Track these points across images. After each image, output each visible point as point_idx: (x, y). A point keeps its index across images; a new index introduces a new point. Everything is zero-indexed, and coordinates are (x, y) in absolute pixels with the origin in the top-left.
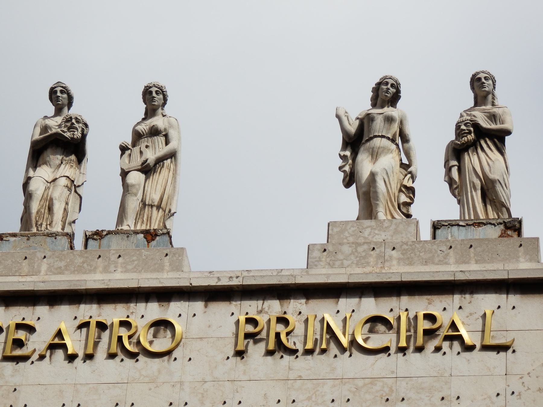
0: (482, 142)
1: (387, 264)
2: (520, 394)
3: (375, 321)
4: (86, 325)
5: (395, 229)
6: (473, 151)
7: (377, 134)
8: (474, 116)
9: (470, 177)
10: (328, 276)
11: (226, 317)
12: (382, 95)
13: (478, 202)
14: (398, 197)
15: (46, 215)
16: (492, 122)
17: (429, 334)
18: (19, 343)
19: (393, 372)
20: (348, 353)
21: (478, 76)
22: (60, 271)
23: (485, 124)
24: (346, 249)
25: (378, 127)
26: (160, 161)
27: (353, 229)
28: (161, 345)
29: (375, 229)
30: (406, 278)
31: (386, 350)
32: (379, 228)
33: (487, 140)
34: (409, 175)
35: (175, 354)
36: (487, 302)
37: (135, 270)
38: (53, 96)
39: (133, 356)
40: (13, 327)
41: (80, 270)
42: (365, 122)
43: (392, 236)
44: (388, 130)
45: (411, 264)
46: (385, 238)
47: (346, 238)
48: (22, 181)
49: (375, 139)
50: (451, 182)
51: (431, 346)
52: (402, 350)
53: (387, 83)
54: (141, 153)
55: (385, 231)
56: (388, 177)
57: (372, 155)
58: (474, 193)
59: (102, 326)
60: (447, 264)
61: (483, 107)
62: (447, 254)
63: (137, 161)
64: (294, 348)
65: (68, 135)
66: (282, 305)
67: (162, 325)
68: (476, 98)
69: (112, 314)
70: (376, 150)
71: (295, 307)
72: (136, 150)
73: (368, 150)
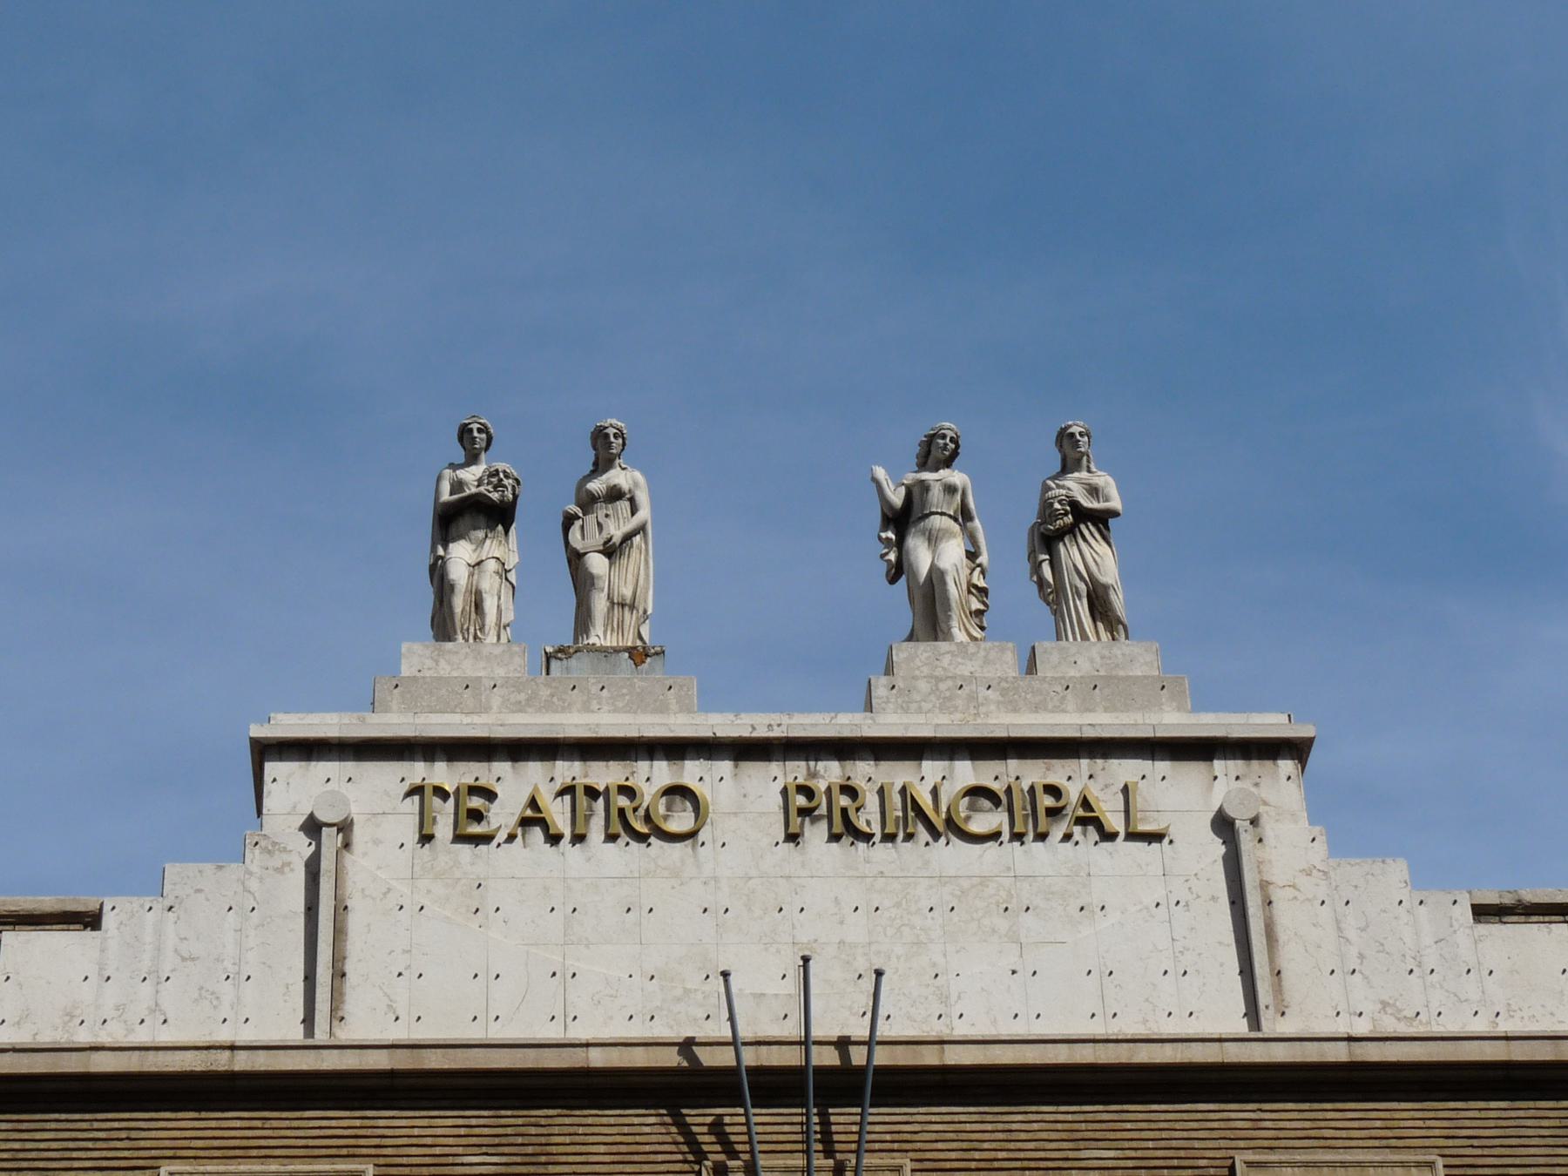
0: (1082, 527)
1: (982, 709)
2: (1187, 905)
3: (976, 792)
9: (1069, 578)
10: (907, 726)
11: (766, 783)
14: (968, 602)
15: (473, 615)
17: (1053, 813)
18: (476, 816)
19: (1009, 869)
20: (943, 840)
22: (520, 708)
23: (1087, 503)
24: (923, 686)
26: (628, 537)
28: (681, 821)
30: (1015, 734)
31: (995, 836)
35: (702, 836)
36: (1126, 769)
37: (627, 709)
38: (466, 436)
39: (641, 838)
40: (464, 791)
41: (548, 707)
44: (949, 504)
45: (1015, 710)
48: (427, 560)
50: (1041, 583)
51: (1058, 832)
52: (1018, 837)
53: (944, 436)
54: (600, 525)
57: (929, 540)
59: (592, 793)
60: (1064, 711)
61: (1076, 475)
62: (1064, 698)
63: (597, 540)
64: (867, 830)
65: (495, 496)
66: (843, 767)
67: (678, 792)
68: (1064, 460)
69: (605, 774)
71: (863, 771)
72: (590, 520)
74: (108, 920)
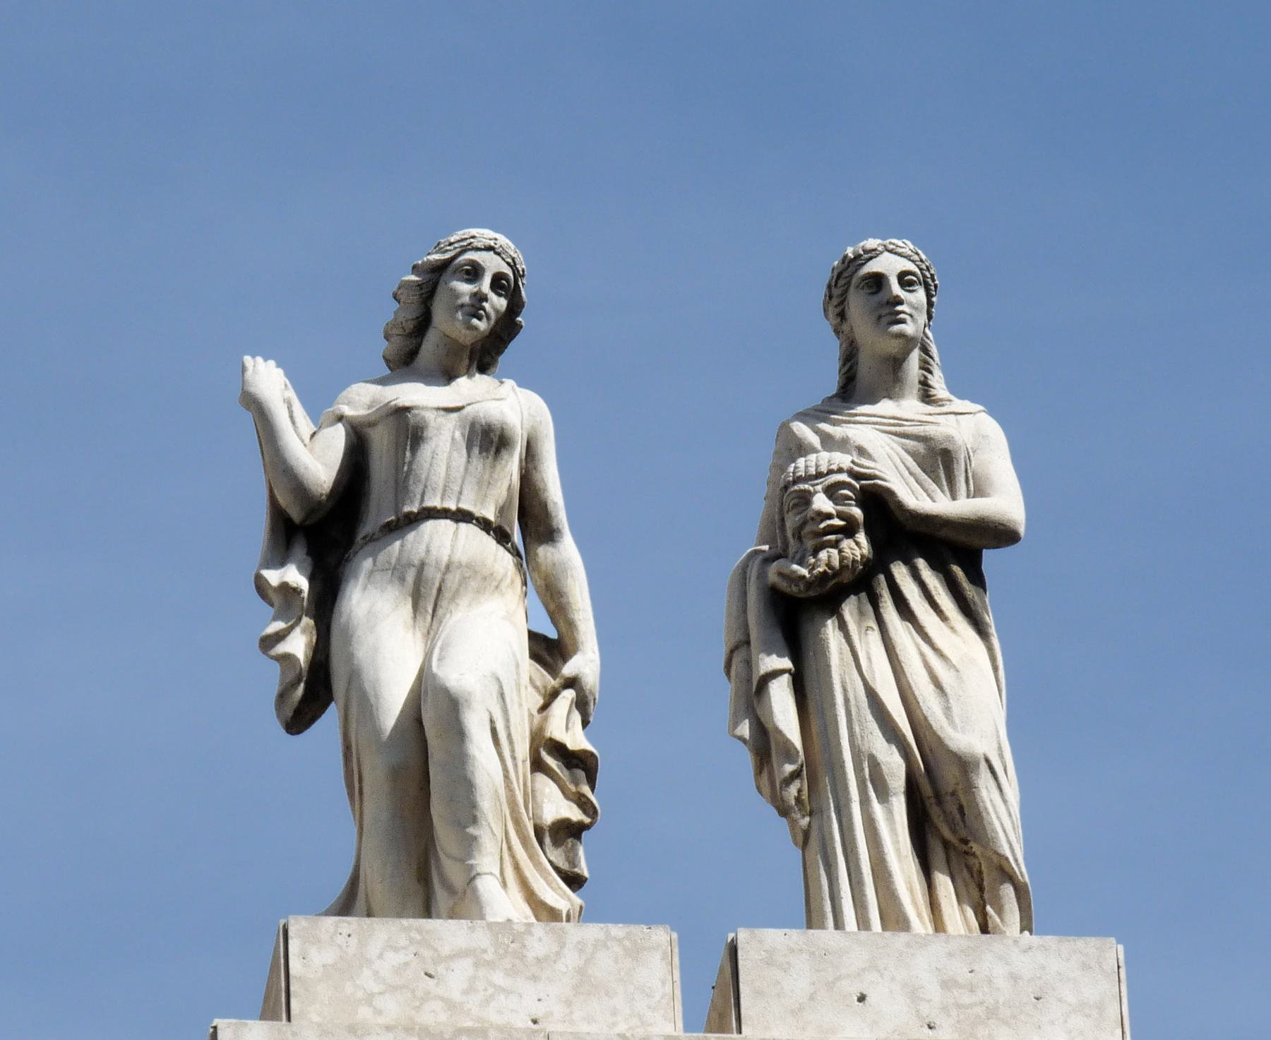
0: (900, 572)
5: (581, 971)
6: (861, 613)
7: (434, 502)
8: (861, 451)
12: (446, 324)
13: (898, 850)
16: (936, 480)
21: (873, 267)
23: (918, 496)
25: (443, 474)
27: (393, 959)
29: (490, 965)
32: (507, 963)
33: (921, 563)
34: (569, 694)
43: (568, 1003)
44: (484, 486)
46: (539, 1010)
47: (369, 999)
49: (429, 526)
53: (474, 273)
55: (535, 978)
56: (505, 711)
57: (417, 598)
58: (877, 808)
61: (885, 407)
70: (433, 575)
73: (397, 572)
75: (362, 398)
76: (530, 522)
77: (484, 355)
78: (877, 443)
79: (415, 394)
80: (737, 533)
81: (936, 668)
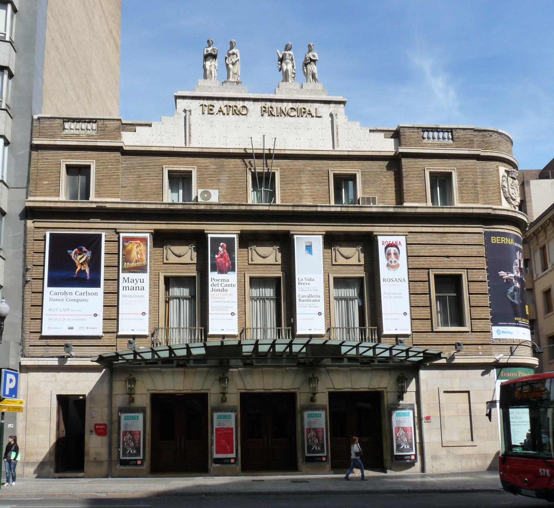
4: (226, 106)
9: (309, 71)
11: (260, 105)
22: (218, 91)
23: (313, 58)
24: (284, 90)
26: (236, 62)
28: (244, 112)
31: (295, 116)
36: (316, 105)
41: (223, 91)
42: (284, 55)
59: (230, 107)
63: (231, 62)
69: (232, 103)
71: (274, 104)
74: (153, 125)
75: (283, 52)
76: (292, 60)
77: (290, 50)
78: (310, 55)
79: (286, 52)
80: (303, 60)
81: (313, 68)
